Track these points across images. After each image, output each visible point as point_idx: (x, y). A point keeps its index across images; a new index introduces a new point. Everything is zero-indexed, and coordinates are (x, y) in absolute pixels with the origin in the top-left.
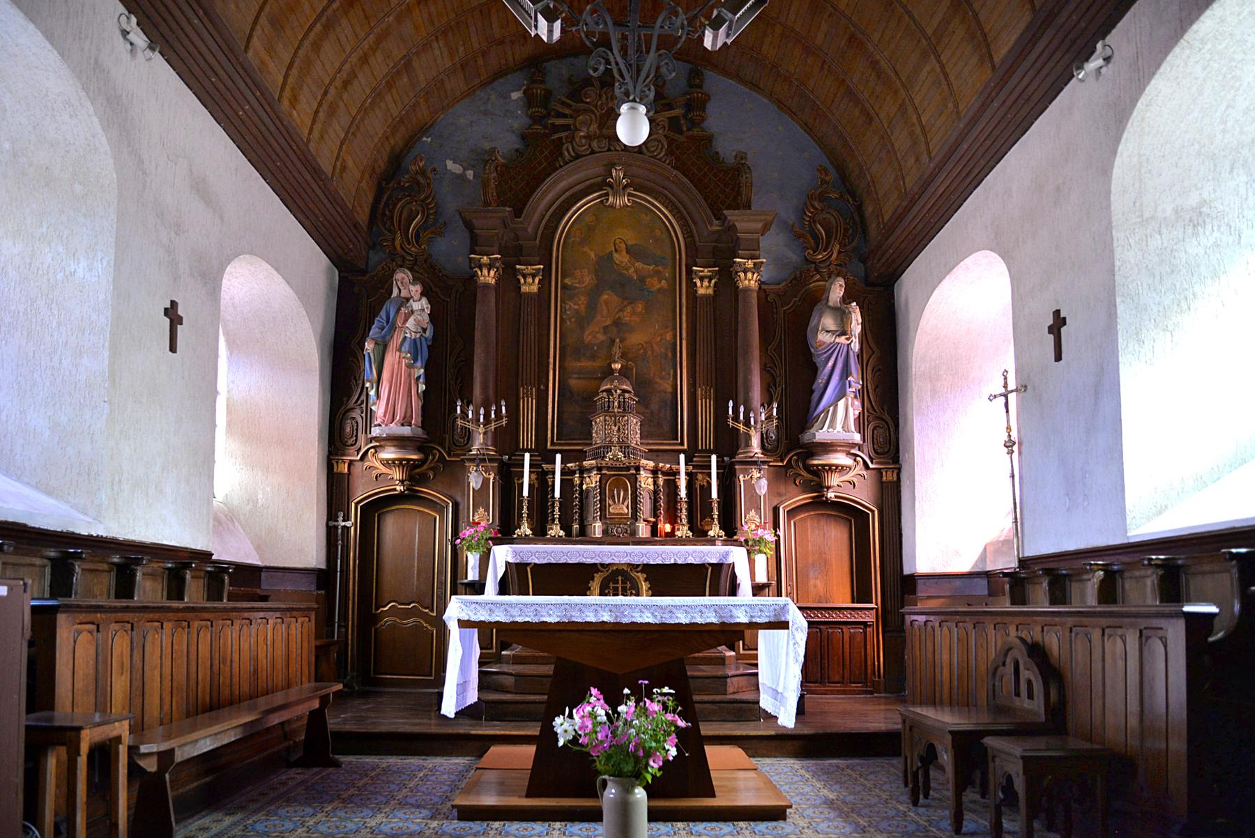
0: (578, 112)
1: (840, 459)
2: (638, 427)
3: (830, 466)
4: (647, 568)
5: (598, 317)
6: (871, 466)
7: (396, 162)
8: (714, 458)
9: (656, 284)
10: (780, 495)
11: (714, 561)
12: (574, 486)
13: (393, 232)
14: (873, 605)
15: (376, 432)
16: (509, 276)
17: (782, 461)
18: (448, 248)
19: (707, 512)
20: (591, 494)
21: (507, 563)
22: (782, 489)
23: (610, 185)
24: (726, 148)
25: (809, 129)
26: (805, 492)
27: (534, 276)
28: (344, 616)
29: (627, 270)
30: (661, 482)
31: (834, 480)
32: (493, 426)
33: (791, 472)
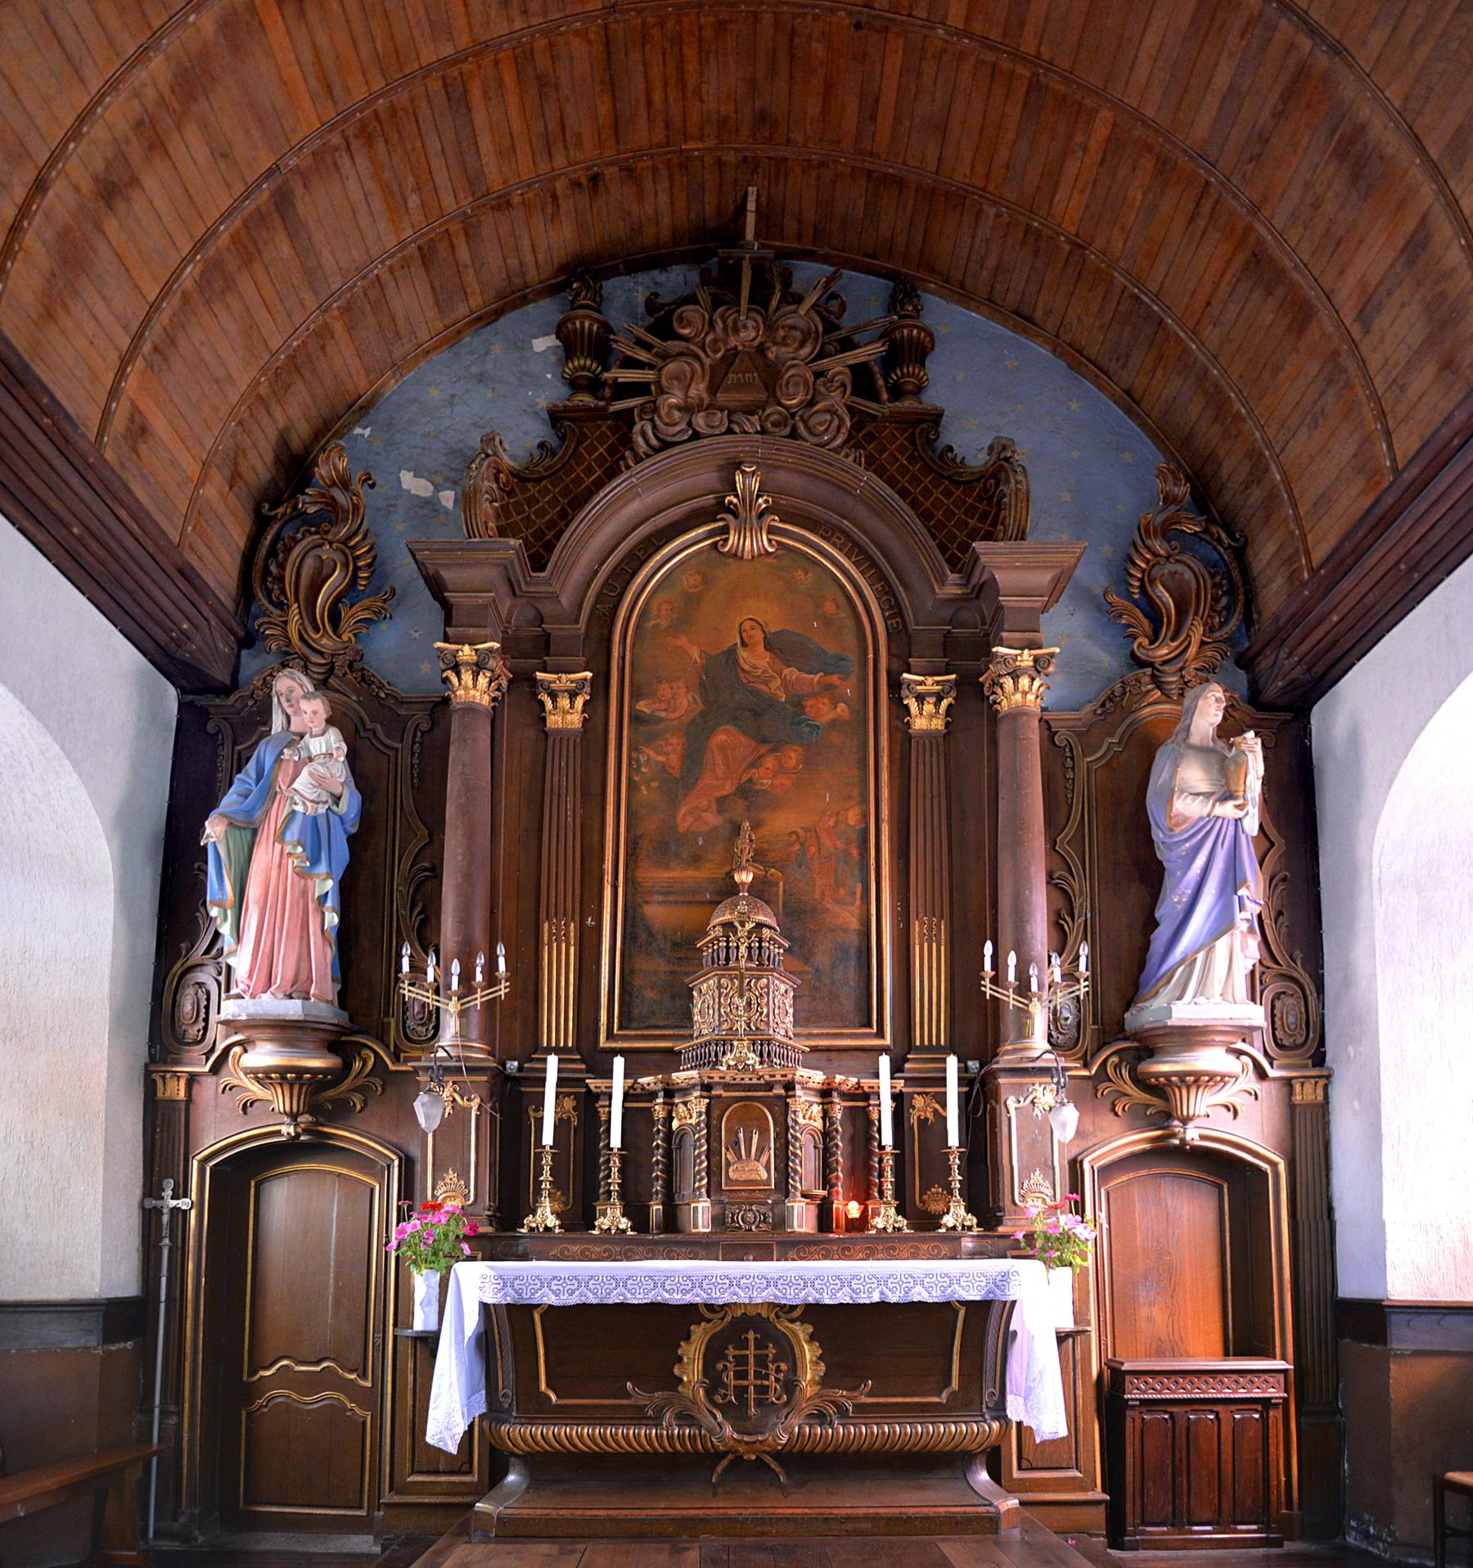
0: (666, 357)
1: (1210, 1059)
2: (789, 1001)
3: (1198, 1075)
4: (814, 1313)
5: (707, 780)
6: (1272, 1073)
7: (295, 468)
9: (825, 712)
11: (974, 1295)
12: (652, 1122)
13: (282, 606)
14: (1278, 1364)
15: (230, 1009)
16: (522, 690)
18: (401, 646)
19: (936, 1171)
20: (690, 1140)
21: (485, 1308)
24: (968, 441)
26: (1134, 1128)
27: (573, 695)
28: (173, 1392)
29: (766, 683)
30: (838, 1112)
33: (1105, 1088)
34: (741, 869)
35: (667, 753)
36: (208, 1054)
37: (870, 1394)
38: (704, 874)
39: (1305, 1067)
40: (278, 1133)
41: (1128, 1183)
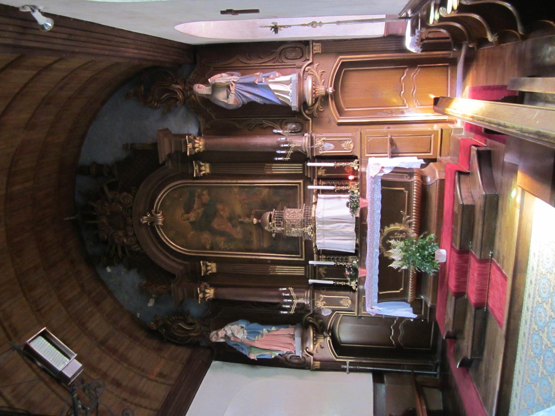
1: (309, 84)
7: (152, 333)
8: (309, 164)
9: (206, 197)
10: (330, 122)
13: (190, 337)
17: (308, 120)
22: (326, 120)
23: (152, 223)
25: (103, 103)
27: (207, 266)
31: (321, 90)
32: (293, 294)
33: (316, 114)
34: (252, 222)
35: (221, 241)
36: (308, 356)
37: (404, 211)
38: (254, 230)
39: (309, 48)
40: (329, 341)
41: (344, 101)
